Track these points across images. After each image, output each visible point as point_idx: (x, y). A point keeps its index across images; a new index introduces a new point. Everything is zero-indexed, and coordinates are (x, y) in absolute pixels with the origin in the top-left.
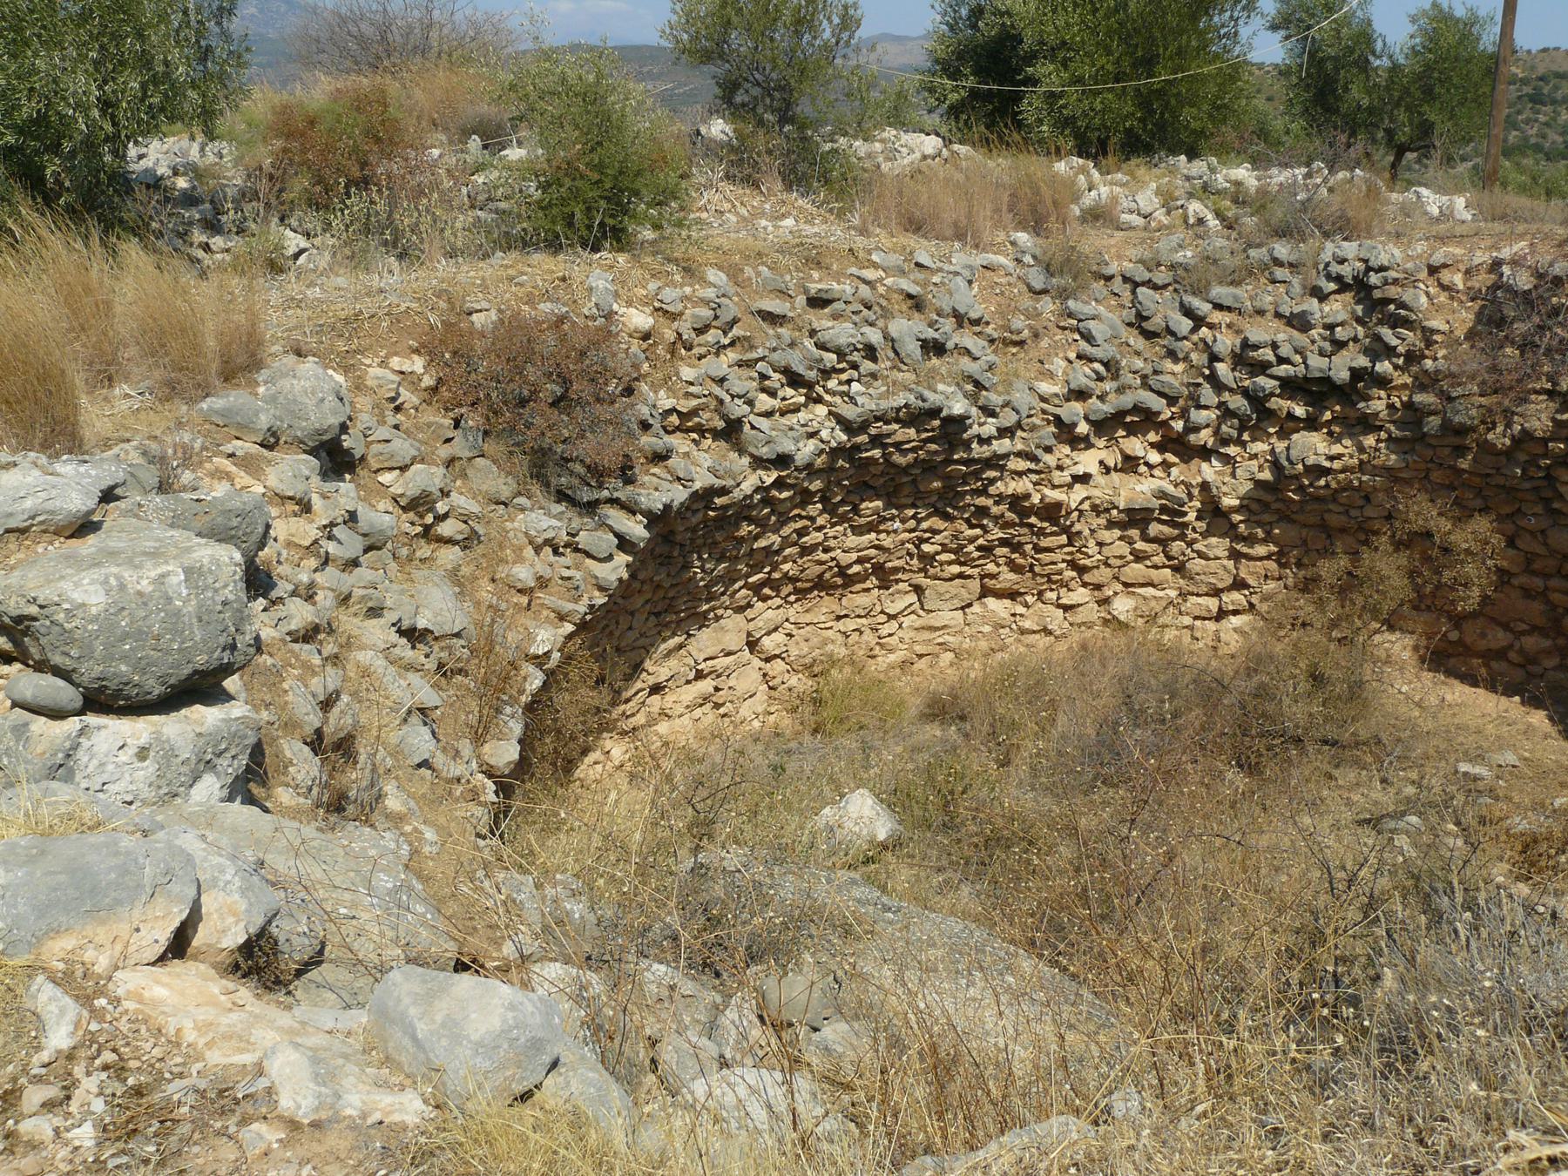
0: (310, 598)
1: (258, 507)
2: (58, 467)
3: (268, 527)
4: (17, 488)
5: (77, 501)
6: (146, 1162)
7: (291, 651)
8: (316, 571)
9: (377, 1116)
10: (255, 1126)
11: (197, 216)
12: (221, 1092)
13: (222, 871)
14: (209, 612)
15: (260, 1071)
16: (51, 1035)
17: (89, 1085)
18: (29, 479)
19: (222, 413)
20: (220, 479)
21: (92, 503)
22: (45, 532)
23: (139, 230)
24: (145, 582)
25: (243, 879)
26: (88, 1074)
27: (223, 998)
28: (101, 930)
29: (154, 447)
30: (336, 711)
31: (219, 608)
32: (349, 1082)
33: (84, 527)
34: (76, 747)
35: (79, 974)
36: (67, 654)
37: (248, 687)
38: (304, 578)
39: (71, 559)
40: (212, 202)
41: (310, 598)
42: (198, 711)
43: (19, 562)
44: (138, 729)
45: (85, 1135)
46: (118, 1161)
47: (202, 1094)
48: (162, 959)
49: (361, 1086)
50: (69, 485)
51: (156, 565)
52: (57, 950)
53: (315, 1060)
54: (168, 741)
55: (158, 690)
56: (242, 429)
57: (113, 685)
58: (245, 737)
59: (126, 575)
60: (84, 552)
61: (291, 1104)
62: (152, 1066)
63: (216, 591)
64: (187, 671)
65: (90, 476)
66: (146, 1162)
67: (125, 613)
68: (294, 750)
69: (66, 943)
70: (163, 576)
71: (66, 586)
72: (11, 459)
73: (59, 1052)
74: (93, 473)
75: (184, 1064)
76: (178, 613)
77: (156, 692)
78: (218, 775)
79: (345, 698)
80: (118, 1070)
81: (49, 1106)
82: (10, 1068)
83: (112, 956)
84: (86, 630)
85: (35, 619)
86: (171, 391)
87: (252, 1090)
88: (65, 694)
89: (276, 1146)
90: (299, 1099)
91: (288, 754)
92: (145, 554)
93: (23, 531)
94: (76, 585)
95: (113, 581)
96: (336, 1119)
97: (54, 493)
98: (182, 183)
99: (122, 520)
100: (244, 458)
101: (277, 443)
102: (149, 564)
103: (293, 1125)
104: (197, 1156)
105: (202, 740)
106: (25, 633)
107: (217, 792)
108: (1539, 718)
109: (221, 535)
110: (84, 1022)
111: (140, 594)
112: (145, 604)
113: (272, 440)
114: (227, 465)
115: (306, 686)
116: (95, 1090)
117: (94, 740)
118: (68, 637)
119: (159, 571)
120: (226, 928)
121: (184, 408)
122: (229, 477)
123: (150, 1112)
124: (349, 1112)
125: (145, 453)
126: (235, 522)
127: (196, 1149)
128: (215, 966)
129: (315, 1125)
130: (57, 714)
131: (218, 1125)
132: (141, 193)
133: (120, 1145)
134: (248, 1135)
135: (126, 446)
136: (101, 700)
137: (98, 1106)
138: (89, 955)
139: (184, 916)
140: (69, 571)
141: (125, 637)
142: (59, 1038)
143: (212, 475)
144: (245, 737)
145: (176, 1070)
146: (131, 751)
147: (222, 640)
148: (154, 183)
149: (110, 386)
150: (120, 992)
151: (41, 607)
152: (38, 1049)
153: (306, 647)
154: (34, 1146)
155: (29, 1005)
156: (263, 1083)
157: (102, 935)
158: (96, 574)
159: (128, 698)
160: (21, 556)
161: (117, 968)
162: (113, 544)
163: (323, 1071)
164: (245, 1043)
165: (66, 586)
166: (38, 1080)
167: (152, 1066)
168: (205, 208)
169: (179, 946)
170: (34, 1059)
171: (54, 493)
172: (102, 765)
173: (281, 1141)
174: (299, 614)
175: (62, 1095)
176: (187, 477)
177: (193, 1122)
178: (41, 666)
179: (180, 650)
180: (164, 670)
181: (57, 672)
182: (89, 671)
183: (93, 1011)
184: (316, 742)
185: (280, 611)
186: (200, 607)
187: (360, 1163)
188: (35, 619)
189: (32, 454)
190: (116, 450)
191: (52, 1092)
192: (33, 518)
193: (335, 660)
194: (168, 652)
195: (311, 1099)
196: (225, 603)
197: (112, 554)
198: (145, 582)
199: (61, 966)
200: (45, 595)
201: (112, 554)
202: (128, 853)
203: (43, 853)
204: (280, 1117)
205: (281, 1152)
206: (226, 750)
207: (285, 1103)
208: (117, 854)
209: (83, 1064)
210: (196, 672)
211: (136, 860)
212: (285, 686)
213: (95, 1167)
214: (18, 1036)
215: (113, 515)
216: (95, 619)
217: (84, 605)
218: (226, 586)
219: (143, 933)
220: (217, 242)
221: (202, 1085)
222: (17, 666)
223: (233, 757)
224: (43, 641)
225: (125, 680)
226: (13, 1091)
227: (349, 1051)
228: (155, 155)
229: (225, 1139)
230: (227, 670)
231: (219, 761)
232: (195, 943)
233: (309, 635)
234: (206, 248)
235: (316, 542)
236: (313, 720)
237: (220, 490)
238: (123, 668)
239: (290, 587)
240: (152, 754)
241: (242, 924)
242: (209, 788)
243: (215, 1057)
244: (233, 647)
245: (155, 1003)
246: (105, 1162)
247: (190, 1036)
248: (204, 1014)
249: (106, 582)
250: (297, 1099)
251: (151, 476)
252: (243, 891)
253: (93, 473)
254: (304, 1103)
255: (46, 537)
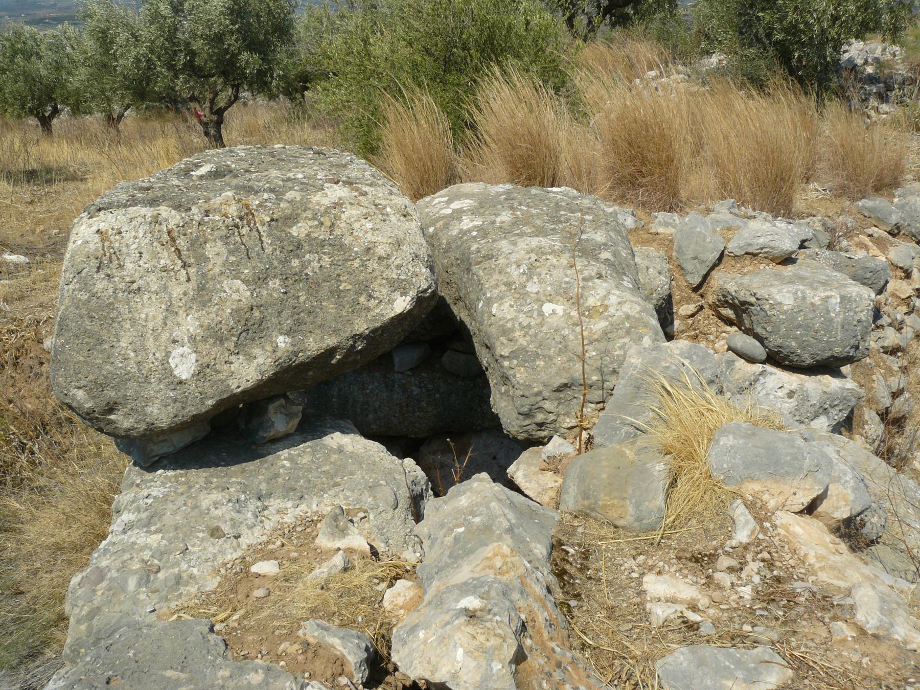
0: (899, 330)
1: (884, 269)
2: (778, 223)
3: (887, 282)
4: (757, 231)
5: (787, 245)
6: (777, 619)
7: (881, 358)
8: (905, 314)
9: (914, 646)
10: (840, 623)
11: (875, 91)
12: (824, 597)
13: (845, 475)
14: (849, 324)
15: (849, 593)
16: (738, 533)
17: (753, 567)
18: (765, 227)
19: (871, 210)
20: (861, 248)
21: (795, 247)
22: (766, 258)
23: (841, 94)
24: (817, 298)
25: (855, 482)
26: (754, 560)
27: (831, 545)
28: (774, 486)
29: (830, 223)
30: (902, 399)
31: (855, 323)
32: (900, 620)
33: (787, 260)
34: (756, 380)
35: (758, 505)
36: (765, 329)
37: (854, 372)
38: (899, 317)
39: (778, 276)
40: (885, 83)
41: (899, 330)
42: (827, 379)
43: (749, 271)
44: (793, 380)
45: (747, 592)
46: (762, 613)
47: (814, 594)
48: (801, 512)
49: (906, 625)
50: (780, 234)
51: (825, 290)
52: (751, 488)
53: (883, 600)
54: (807, 391)
55: (809, 361)
56: (880, 221)
57: (785, 352)
58: (850, 401)
59: (808, 292)
60: (786, 274)
61: (863, 619)
62: (788, 569)
63: (856, 313)
64: (828, 354)
65: (793, 232)
66: (777, 619)
67: (802, 313)
68: (870, 416)
69: (755, 487)
70: (828, 297)
71: (774, 290)
72: (753, 214)
73: (741, 543)
74: (796, 230)
75: (805, 574)
76: (831, 320)
77: (808, 362)
78: (828, 418)
79: (907, 395)
80: (770, 564)
81: (731, 570)
82: (714, 542)
83: (777, 502)
84: (778, 318)
85: (752, 305)
86: (842, 192)
87: (842, 603)
88: (758, 350)
89: (850, 639)
90: (869, 618)
91: (866, 417)
92: (821, 283)
93: (755, 255)
94: (779, 291)
95: (799, 294)
96: (888, 638)
97: (776, 237)
98: (870, 70)
99: (808, 261)
100: (878, 239)
101: (898, 233)
102: (821, 289)
103: (862, 631)
104: (804, 627)
105: (826, 396)
106: (744, 311)
107: (825, 428)
108: (160, 471)
109: (864, 282)
110: (756, 532)
111: (813, 304)
112: (814, 311)
113: (896, 231)
114: (867, 240)
115: (886, 381)
116: (756, 570)
117: (767, 379)
118: (768, 319)
119: (827, 294)
120: (839, 507)
121: (848, 203)
122: (867, 248)
123: (783, 594)
124: (896, 637)
125: (824, 225)
126: (868, 275)
127: (804, 623)
128: (827, 525)
129: (875, 636)
130: (751, 360)
131: (819, 614)
132: (844, 74)
133: (765, 605)
134: (835, 627)
135: (814, 219)
136: (776, 359)
137: (757, 579)
138: (766, 497)
139: (820, 493)
140: (776, 283)
141: (799, 326)
142: (742, 536)
143: (857, 245)
144: (850, 401)
145: (801, 576)
146: (785, 391)
147: (852, 342)
148: (853, 68)
149: (807, 183)
150: (778, 523)
151: (758, 299)
152: (730, 538)
153: (892, 358)
154: (719, 587)
155: (731, 513)
156: (849, 601)
157: (774, 487)
158: (791, 288)
159: (791, 361)
160: (751, 268)
161: (778, 509)
162: (802, 273)
163: (886, 608)
164: (842, 575)
165: (774, 290)
166: (727, 554)
167: (788, 569)
168: (883, 85)
169: (810, 509)
170: (728, 542)
171: (776, 237)
172: (768, 394)
173: (853, 637)
174: (891, 337)
175: (739, 566)
176: (844, 243)
177: (805, 607)
178: (749, 332)
179: (827, 342)
180: (815, 350)
181: (757, 337)
182: (775, 341)
183: (762, 527)
184: (884, 415)
185: (880, 333)
186: (845, 319)
187: (899, 669)
188: (752, 305)
189: (765, 213)
190: (808, 220)
191: (734, 563)
192: (762, 249)
193: (904, 370)
194: (820, 341)
195: (876, 621)
196: (859, 321)
197: (802, 279)
198: (817, 298)
199: (751, 498)
200: (761, 293)
201: (802, 279)
202: (799, 448)
203: (754, 434)
204: (855, 624)
205: (852, 644)
206: (837, 405)
207: (860, 617)
208: (793, 447)
209: (752, 554)
210: (833, 356)
211: (802, 453)
212: (874, 377)
213: (749, 611)
214: (721, 527)
215: (802, 256)
216: (785, 313)
217: (781, 303)
218: (862, 311)
219: (797, 496)
220: (885, 107)
221: (815, 589)
222: (735, 328)
223: (840, 410)
224: (754, 318)
225: (792, 350)
226: (714, 555)
227: (901, 602)
228: (855, 51)
229: (821, 624)
230: (849, 360)
231: (832, 410)
232: (819, 509)
233: (893, 351)
234: (877, 110)
235: (909, 297)
236: (887, 401)
237: (860, 254)
238: (793, 344)
239: (889, 321)
240: (796, 396)
241: (849, 508)
242: (822, 424)
243: (823, 577)
244: (857, 348)
245: (795, 535)
246: (755, 610)
247: (811, 560)
248: (821, 551)
249: (796, 293)
250: (868, 615)
251: (825, 238)
252: (855, 489)
253: (796, 230)
254: (871, 621)
255: (766, 261)
